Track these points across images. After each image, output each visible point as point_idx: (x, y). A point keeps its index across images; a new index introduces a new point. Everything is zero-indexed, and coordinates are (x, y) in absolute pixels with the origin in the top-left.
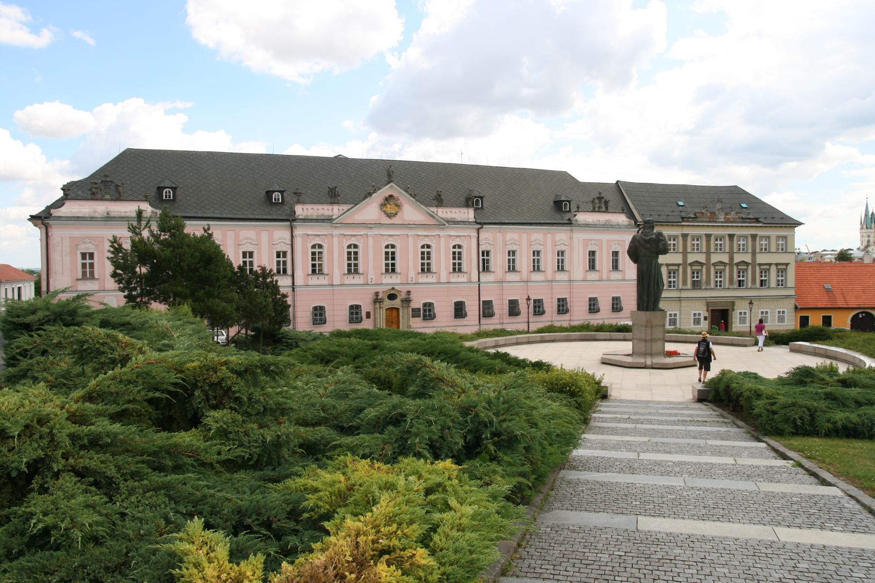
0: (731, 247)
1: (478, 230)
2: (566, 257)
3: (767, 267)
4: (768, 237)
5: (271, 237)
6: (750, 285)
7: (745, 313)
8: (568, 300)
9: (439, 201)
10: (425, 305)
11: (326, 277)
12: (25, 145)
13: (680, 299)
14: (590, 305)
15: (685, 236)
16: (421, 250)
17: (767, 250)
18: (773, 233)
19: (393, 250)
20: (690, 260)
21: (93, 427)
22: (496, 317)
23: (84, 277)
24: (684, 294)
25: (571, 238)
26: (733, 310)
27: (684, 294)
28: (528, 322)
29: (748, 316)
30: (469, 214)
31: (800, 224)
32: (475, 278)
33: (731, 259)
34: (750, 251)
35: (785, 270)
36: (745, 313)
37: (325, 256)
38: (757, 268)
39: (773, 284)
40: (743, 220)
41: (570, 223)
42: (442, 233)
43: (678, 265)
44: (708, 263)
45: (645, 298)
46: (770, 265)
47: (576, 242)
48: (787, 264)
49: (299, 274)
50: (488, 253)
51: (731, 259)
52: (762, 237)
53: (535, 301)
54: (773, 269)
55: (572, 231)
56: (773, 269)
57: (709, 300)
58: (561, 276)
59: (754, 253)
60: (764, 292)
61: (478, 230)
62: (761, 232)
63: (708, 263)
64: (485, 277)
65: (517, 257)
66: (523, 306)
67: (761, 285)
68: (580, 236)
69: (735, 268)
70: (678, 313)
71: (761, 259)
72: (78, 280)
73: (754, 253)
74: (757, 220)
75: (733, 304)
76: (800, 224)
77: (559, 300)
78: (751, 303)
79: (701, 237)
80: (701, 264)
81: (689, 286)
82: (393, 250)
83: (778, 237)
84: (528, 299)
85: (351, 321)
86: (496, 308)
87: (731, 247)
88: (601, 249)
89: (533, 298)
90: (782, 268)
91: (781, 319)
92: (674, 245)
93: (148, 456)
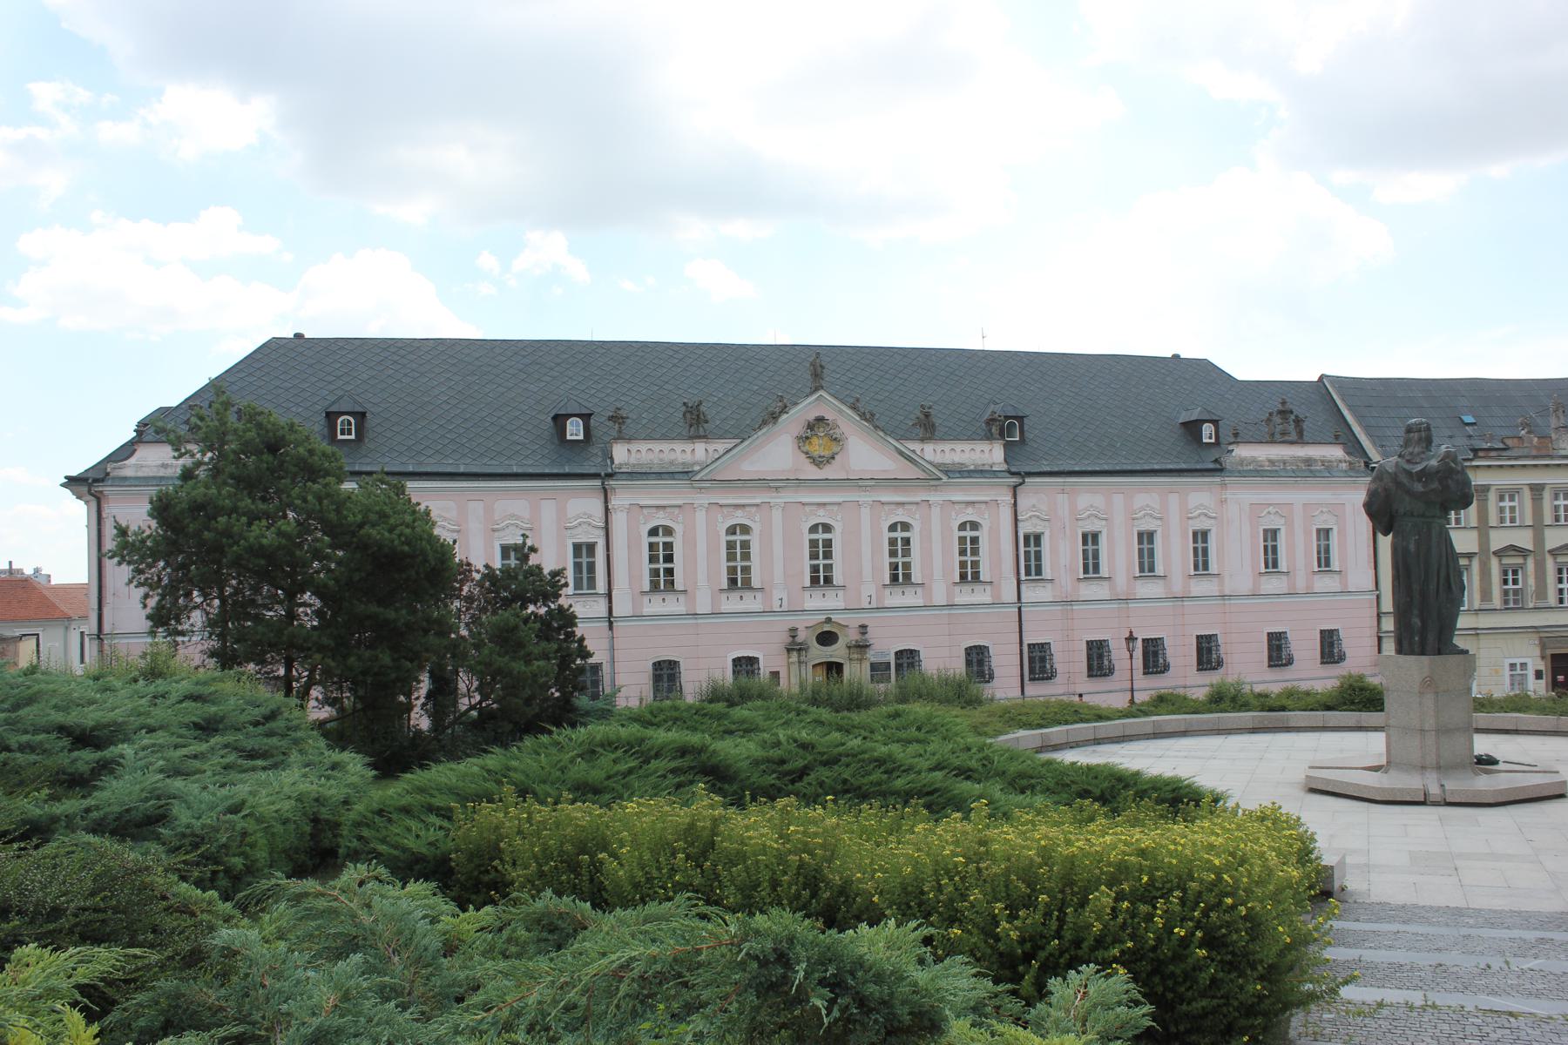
10: (899, 654)
19: (905, 534)
20: (1496, 545)
30: (993, 454)
37: (984, 545)
50: (1038, 538)
64: (1029, 593)
66: (1118, 653)
72: (643, 593)
80: (1523, 552)
82: (905, 534)
89: (1141, 635)
92: (1512, 509)
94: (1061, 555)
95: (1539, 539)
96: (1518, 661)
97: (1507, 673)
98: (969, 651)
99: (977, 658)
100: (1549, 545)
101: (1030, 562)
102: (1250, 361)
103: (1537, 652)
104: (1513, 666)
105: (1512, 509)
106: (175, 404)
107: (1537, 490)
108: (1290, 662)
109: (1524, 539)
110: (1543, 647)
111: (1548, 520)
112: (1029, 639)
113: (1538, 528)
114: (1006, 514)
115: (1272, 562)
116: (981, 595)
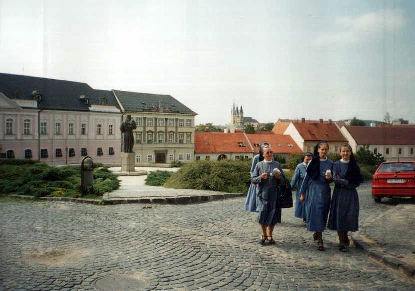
0: (166, 124)
1: (39, 112)
2: (113, 128)
3: (182, 134)
4: (183, 120)
5: (67, 118)
6: (142, 142)
7: (172, 155)
8: (87, 149)
9: (18, 96)
10: (8, 151)
11: (14, 136)
12: (304, 119)
13: (142, 148)
14: (98, 152)
15: (145, 118)
16: (24, 122)
17: (182, 126)
18: (185, 118)
19: (28, 122)
20: (158, 130)
21: (41, 189)
22: (49, 157)
23: (25, 133)
24: (144, 146)
25: (88, 118)
26: (167, 154)
27: (144, 146)
28: (66, 161)
29: (173, 156)
30: (34, 104)
31: (197, 114)
32: (37, 138)
33: (166, 129)
34: (175, 126)
35: (190, 135)
36: (172, 155)
37: (13, 125)
38: (178, 134)
39: (185, 142)
40: (172, 112)
41: (89, 111)
42: (18, 113)
43: (141, 132)
44: (155, 132)
45: (127, 147)
46: (183, 133)
47: (91, 119)
48: (191, 133)
49: (105, 135)
50: (45, 124)
51: (166, 129)
52: (180, 120)
53: (70, 149)
54: (185, 135)
55: (89, 114)
56: (185, 135)
57: (156, 149)
58: (83, 137)
59: (176, 127)
60: (181, 145)
61: (39, 112)
62: (180, 118)
63: (176, 132)
64: (42, 137)
65: (61, 127)
66: (63, 152)
67: (159, 142)
68: (93, 117)
69: (168, 134)
70: (141, 155)
71: (180, 130)
72: (5, 134)
73: (176, 127)
74: (178, 112)
75: (167, 151)
76: (197, 114)
77: (82, 149)
78: (175, 151)
79: (141, 118)
80: (152, 132)
81: (146, 142)
82: (28, 122)
83: (187, 120)
84: (66, 149)
85: (26, 157)
86: (49, 153)
87: (166, 124)
88: (103, 123)
89: (69, 147)
90: (189, 135)
91: (188, 158)
92: (139, 122)
93: (58, 199)
94: (51, 129)
95: (156, 129)
96: (171, 154)
97: (148, 157)
98: (26, 151)
99: (28, 153)
100: (147, 130)
101: (42, 132)
102: (97, 84)
103: (154, 153)
104: (149, 156)
105: (139, 122)
106: (94, 88)
107: (177, 120)
108: (74, 155)
109: (174, 130)
110: (155, 152)
111: (178, 126)
112: (42, 148)
113: (156, 127)
114: (36, 118)
115: (99, 133)
116: (30, 137)
